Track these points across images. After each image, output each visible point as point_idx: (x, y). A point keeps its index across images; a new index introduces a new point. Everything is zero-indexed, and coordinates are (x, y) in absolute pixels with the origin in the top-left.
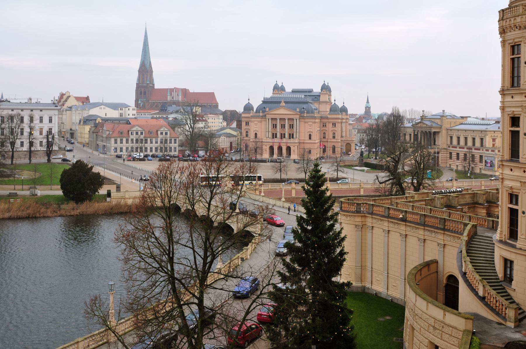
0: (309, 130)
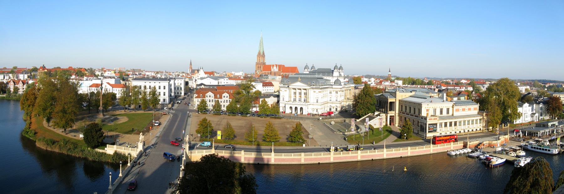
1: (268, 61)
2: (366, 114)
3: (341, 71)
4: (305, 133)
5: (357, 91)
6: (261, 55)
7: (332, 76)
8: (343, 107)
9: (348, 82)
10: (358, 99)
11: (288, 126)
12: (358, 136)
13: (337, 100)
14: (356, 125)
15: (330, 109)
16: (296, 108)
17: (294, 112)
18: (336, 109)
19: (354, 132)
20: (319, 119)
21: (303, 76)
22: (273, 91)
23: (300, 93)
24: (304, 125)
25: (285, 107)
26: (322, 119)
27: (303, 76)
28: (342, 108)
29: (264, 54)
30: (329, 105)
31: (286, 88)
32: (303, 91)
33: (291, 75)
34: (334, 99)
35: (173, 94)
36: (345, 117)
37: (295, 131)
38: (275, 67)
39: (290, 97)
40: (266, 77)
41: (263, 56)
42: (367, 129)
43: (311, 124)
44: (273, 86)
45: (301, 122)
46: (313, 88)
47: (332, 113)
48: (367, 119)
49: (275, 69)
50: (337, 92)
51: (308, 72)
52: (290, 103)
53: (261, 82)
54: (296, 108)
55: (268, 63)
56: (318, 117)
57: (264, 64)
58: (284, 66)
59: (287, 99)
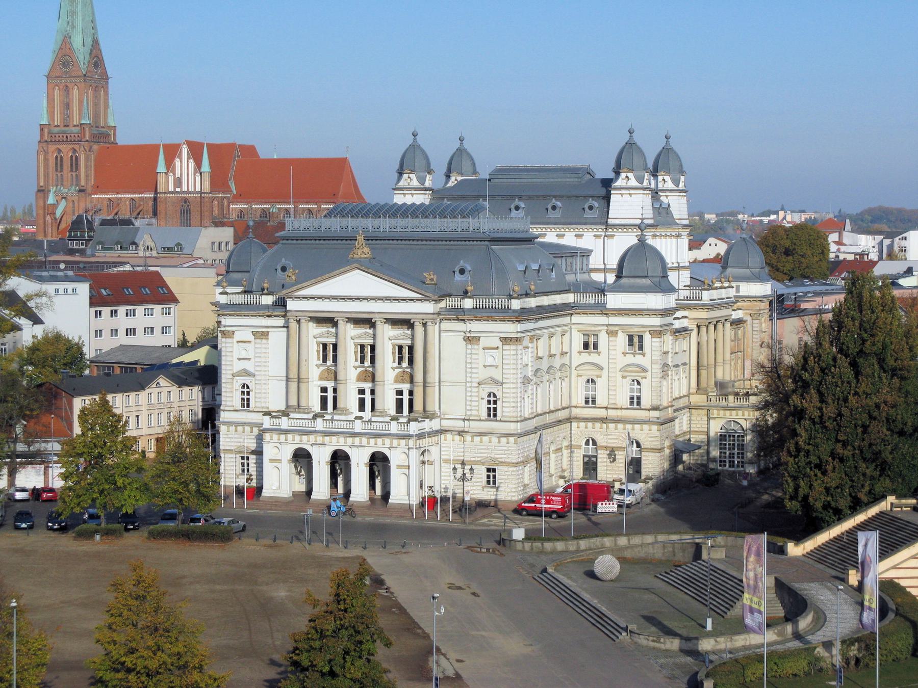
0: (483, 374)
1: (132, 120)
2: (856, 506)
3: (666, 181)
4: (404, 645)
5: (793, 334)
6: (81, 71)
7: (603, 221)
8: (690, 447)
9: (722, 261)
10: (791, 388)
11: (281, 593)
12: (801, 665)
13: (635, 401)
14: (782, 588)
15: (590, 466)
16: (339, 460)
17: (321, 489)
18: (635, 465)
19: (762, 639)
20: (503, 541)
21: (385, 224)
22: (171, 340)
23: (368, 353)
24: (400, 587)
25: (266, 453)
26: (531, 536)
27: (385, 224)
28: (676, 458)
29: (97, 61)
30: (580, 432)
31: (267, 311)
32: (388, 339)
33: (300, 218)
34: (614, 392)
35: (70, 273)
36: (698, 526)
37: (329, 626)
38: (184, 165)
39: (294, 378)
40: (115, 232)
41: (96, 74)
42: (870, 617)
43: (450, 577)
44: (169, 298)
45: (377, 560)
46: (458, 314)
47: (605, 492)
48: (868, 543)
49: (187, 177)
50: (635, 342)
51: (421, 199)
52: (298, 420)
53: (79, 272)
54: (339, 460)
55: (130, 126)
56: (494, 522)
57: (102, 136)
58: (249, 151)
59: (272, 395)
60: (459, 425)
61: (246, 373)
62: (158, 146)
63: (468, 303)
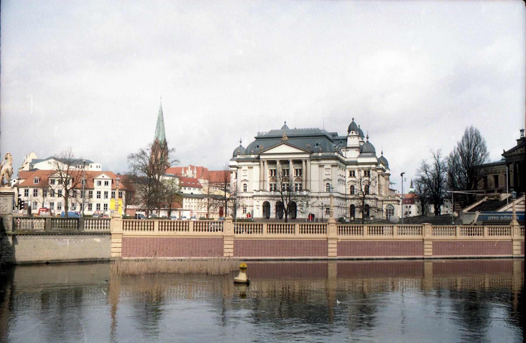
0: (326, 177)
46: (317, 159)
58: (206, 169)
60: (317, 195)
61: (245, 180)
62: (182, 168)
63: (320, 154)
